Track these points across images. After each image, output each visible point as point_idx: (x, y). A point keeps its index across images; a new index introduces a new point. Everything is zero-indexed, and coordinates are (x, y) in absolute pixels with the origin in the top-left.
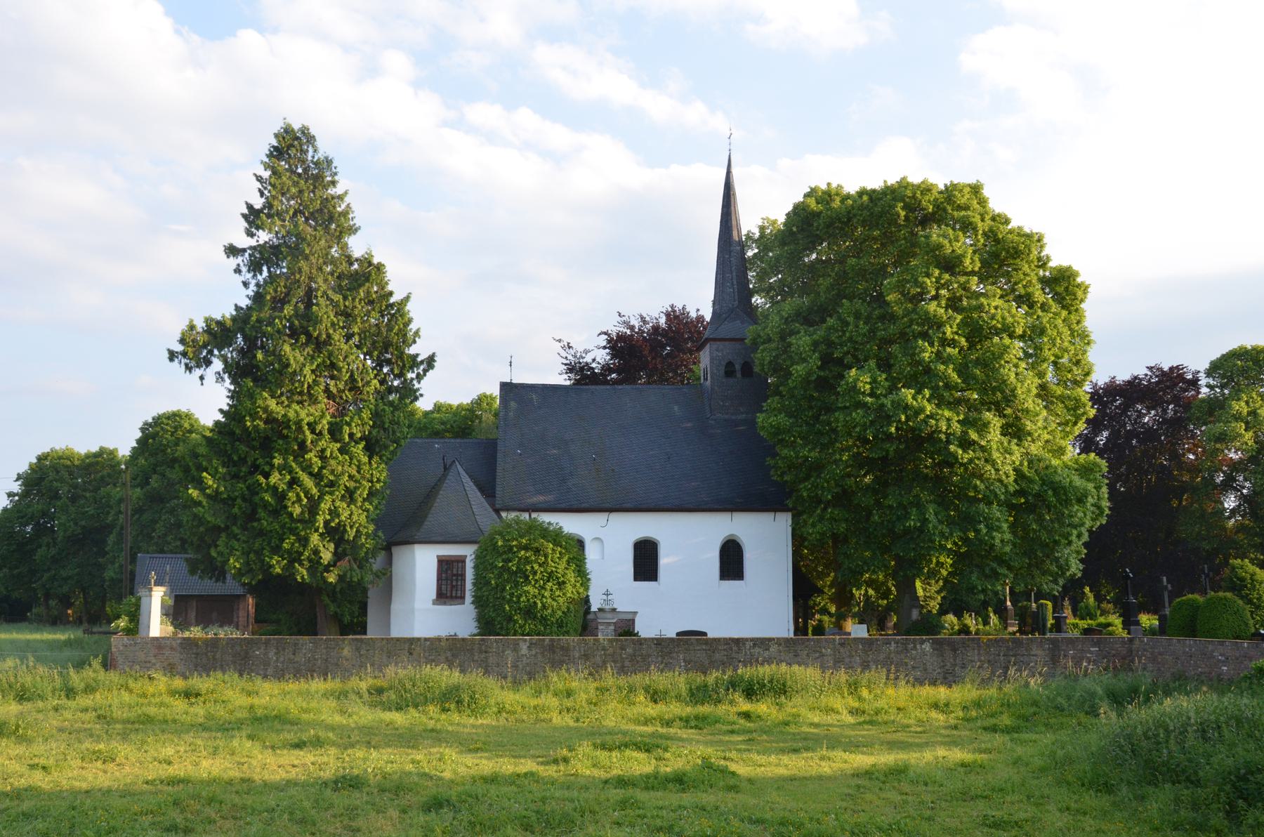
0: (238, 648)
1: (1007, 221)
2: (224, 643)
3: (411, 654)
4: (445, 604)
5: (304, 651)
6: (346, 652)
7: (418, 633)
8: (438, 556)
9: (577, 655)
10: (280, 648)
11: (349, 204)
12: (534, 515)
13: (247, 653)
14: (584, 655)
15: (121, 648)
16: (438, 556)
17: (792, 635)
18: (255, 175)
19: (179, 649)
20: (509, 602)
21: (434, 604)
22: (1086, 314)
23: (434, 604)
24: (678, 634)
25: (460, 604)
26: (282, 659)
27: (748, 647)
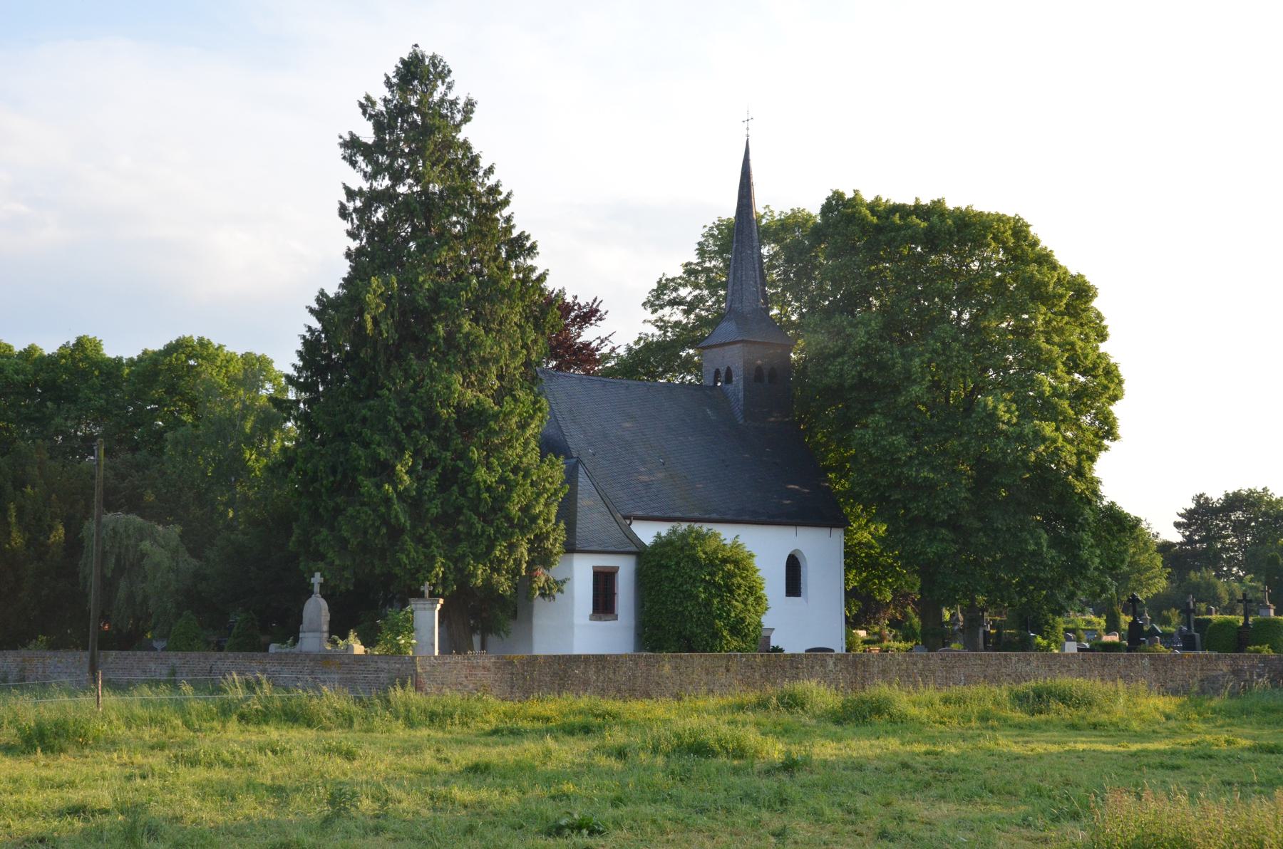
0: (556, 666)
1: (1102, 336)
2: (542, 661)
3: (728, 671)
4: (600, 619)
5: (625, 669)
6: (667, 669)
7: (576, 652)
8: (594, 567)
9: (876, 670)
10: (600, 666)
11: (534, 243)
12: (696, 526)
13: (565, 671)
14: (882, 671)
15: (428, 668)
16: (594, 567)
17: (844, 652)
18: (344, 184)
19: (493, 669)
20: (720, 617)
21: (590, 620)
22: (1125, 392)
23: (590, 620)
24: (807, 651)
25: (614, 620)
26: (602, 678)
27: (1013, 662)
